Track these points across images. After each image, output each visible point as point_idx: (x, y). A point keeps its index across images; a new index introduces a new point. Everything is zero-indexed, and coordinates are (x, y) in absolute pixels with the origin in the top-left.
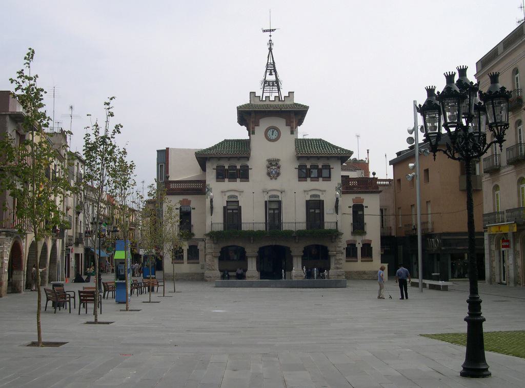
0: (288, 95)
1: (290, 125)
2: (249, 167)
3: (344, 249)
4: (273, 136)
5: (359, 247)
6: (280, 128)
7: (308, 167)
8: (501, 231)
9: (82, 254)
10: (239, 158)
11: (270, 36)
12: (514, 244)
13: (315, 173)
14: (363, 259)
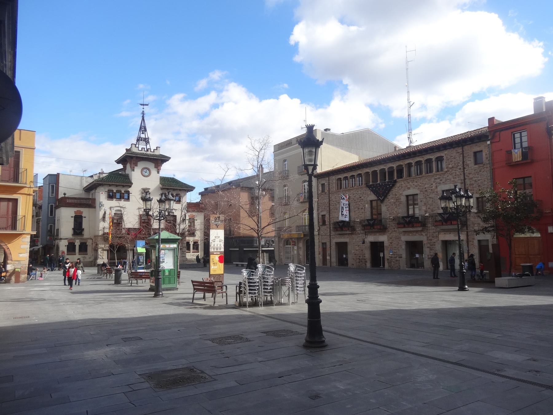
0: (156, 149)
1: (157, 168)
2: (130, 192)
4: (146, 173)
5: (191, 244)
6: (151, 169)
7: (122, 192)
8: (292, 237)
10: (123, 186)
11: (143, 108)
12: (298, 243)
13: (118, 195)
14: (80, 253)
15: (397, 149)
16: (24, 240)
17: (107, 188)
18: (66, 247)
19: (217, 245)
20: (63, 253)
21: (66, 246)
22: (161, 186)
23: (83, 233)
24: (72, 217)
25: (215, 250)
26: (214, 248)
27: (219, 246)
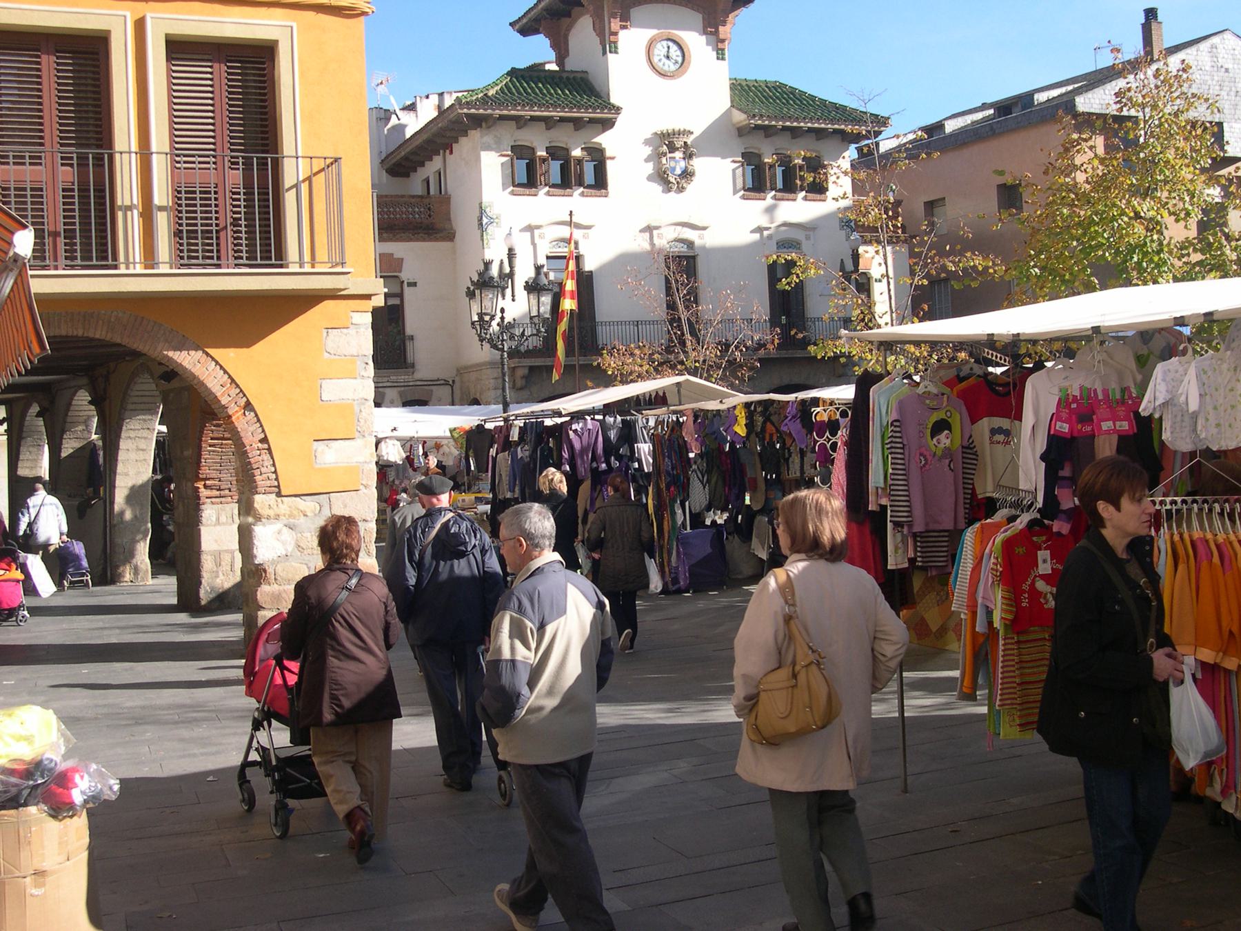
2: (608, 154)
10: (578, 123)
16: (335, 341)
17: (510, 135)
22: (739, 117)
23: (409, 360)
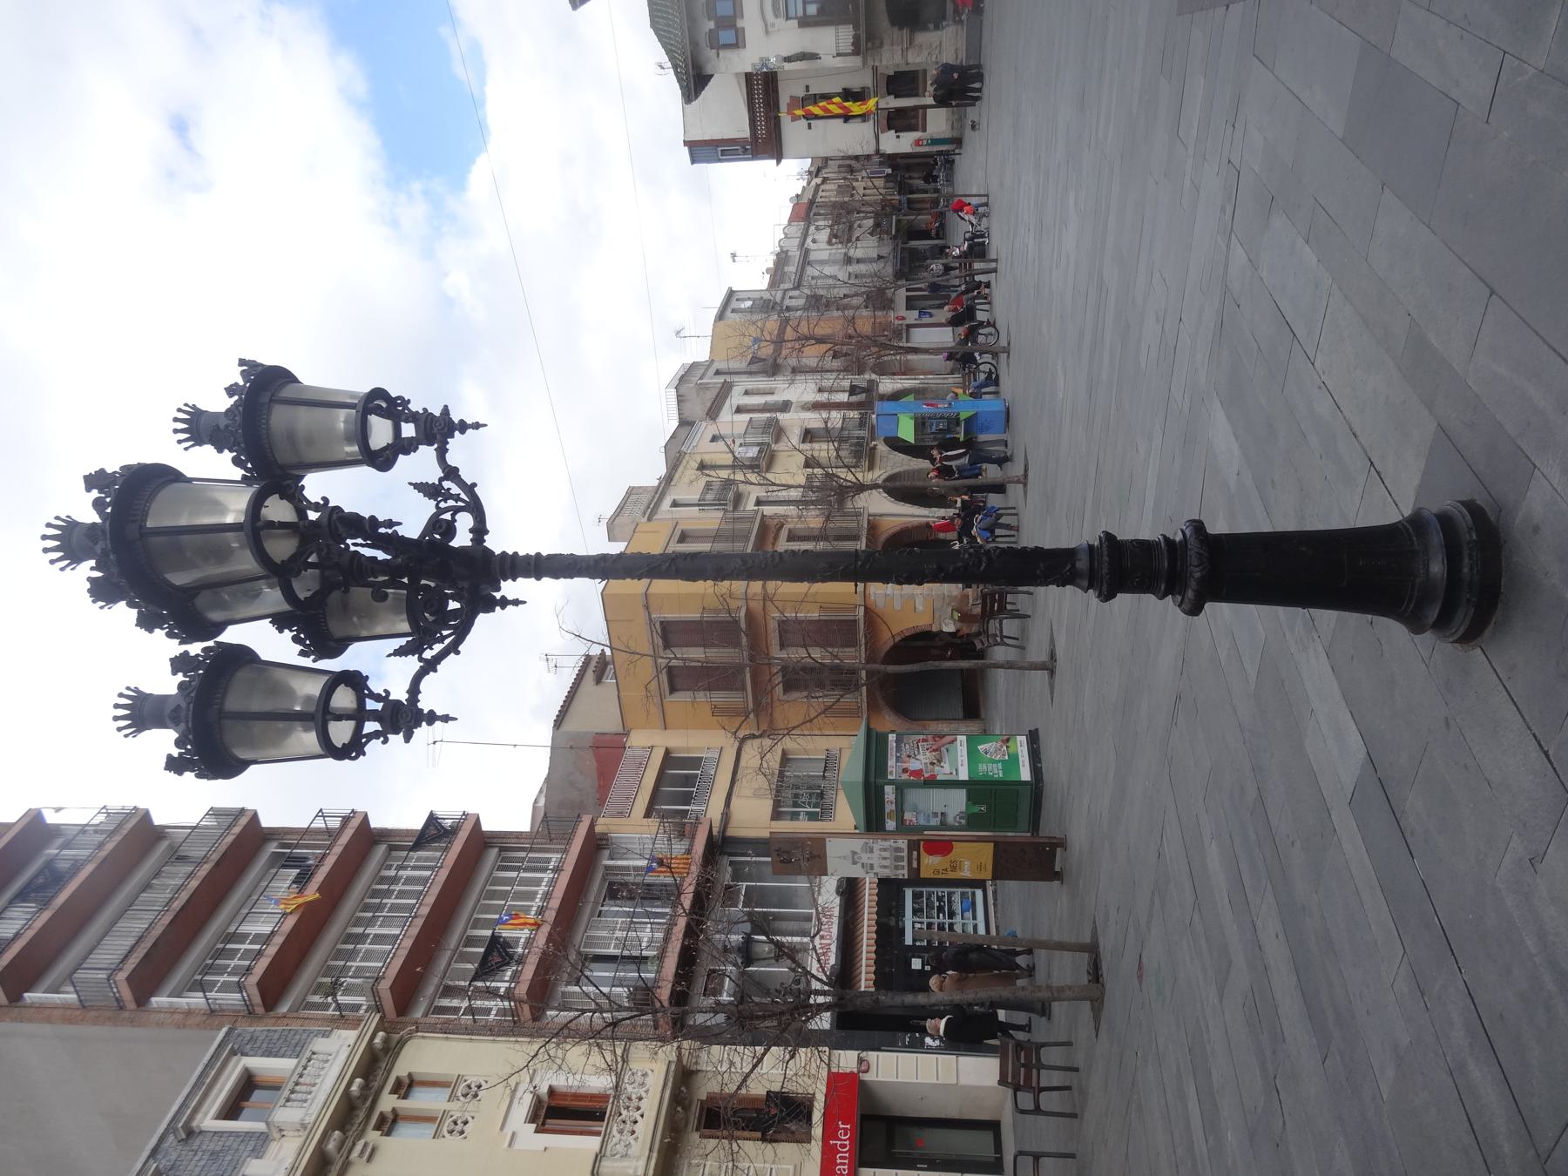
3: (898, 137)
9: (908, 290)
15: (382, 739)
18: (901, 134)
19: (885, 859)
20: (921, 143)
21: (898, 137)
24: (810, 126)
25: (905, 863)
26: (897, 868)
27: (886, 854)
